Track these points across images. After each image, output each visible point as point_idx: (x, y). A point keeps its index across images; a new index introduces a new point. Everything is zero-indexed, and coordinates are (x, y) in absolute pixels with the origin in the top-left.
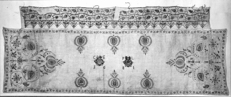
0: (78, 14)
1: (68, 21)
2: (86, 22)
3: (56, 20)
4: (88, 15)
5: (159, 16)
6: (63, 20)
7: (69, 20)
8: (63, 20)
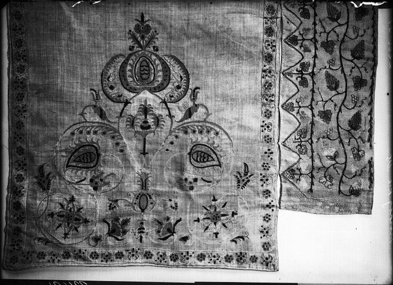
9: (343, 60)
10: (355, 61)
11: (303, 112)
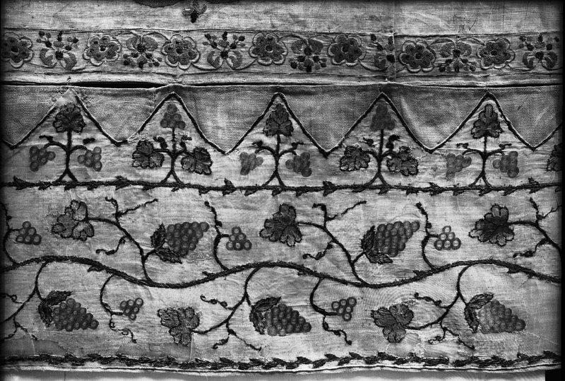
0: (226, 272)
1: (356, 189)
2: (120, 183)
3: (509, 190)
4: (95, 266)
5: (459, 255)
6: (411, 190)
7: (337, 202)
8: (422, 198)
9: (247, 272)
10: (460, 306)
11: (469, 161)
